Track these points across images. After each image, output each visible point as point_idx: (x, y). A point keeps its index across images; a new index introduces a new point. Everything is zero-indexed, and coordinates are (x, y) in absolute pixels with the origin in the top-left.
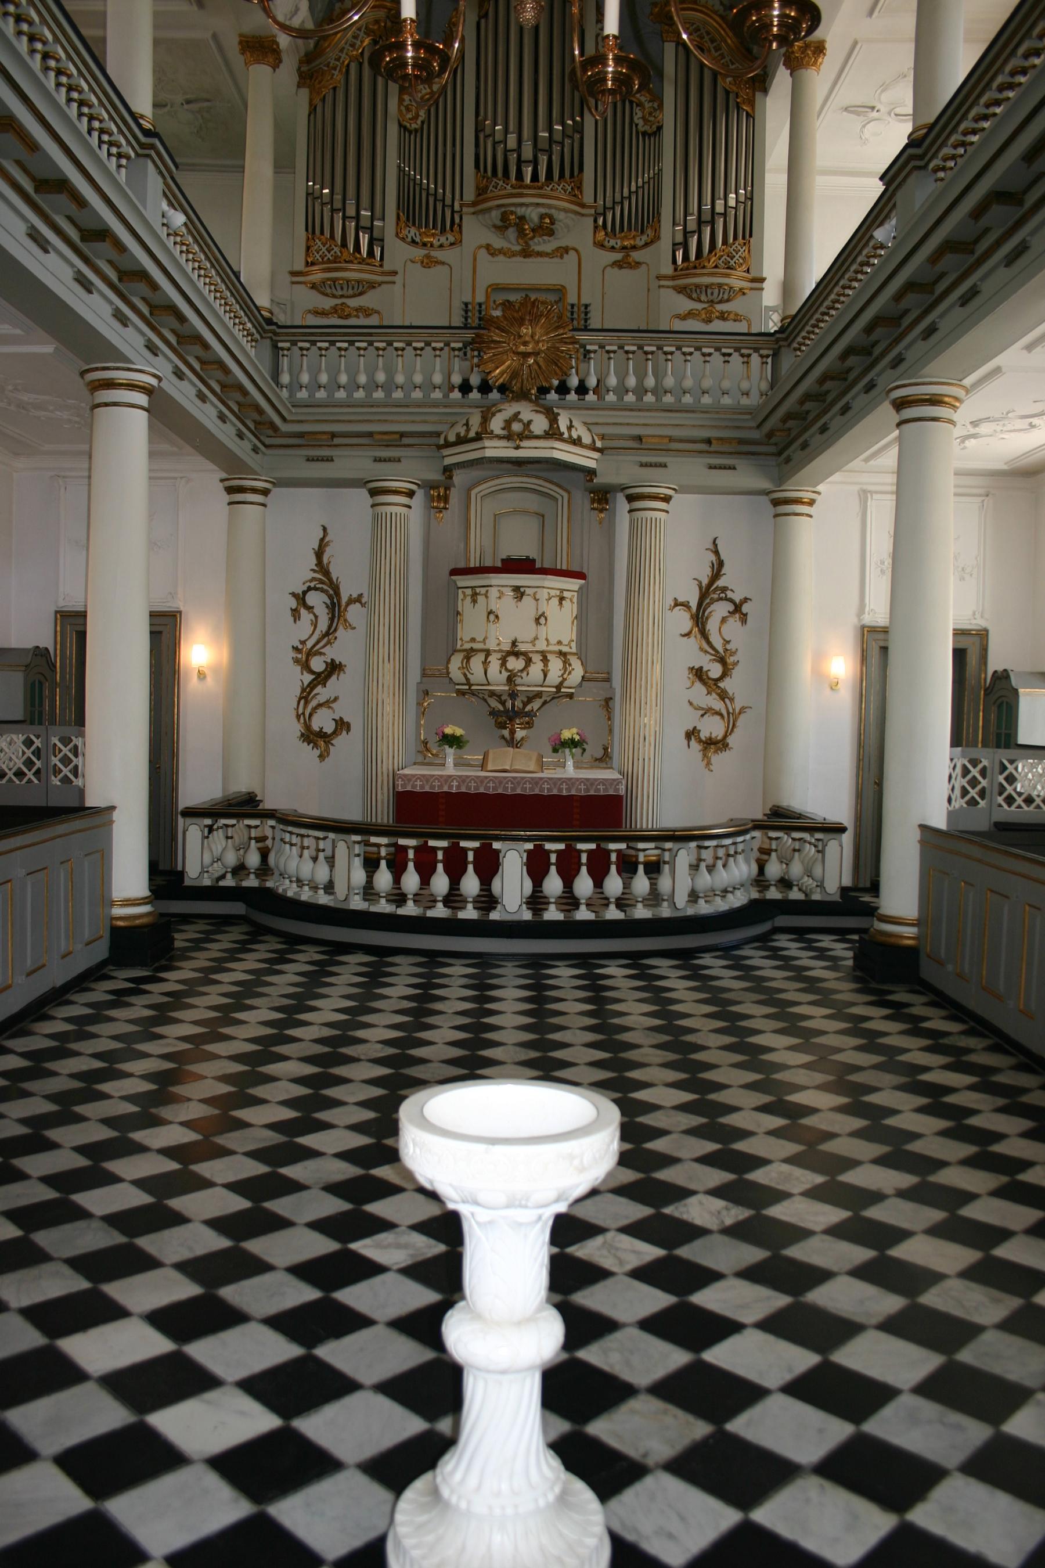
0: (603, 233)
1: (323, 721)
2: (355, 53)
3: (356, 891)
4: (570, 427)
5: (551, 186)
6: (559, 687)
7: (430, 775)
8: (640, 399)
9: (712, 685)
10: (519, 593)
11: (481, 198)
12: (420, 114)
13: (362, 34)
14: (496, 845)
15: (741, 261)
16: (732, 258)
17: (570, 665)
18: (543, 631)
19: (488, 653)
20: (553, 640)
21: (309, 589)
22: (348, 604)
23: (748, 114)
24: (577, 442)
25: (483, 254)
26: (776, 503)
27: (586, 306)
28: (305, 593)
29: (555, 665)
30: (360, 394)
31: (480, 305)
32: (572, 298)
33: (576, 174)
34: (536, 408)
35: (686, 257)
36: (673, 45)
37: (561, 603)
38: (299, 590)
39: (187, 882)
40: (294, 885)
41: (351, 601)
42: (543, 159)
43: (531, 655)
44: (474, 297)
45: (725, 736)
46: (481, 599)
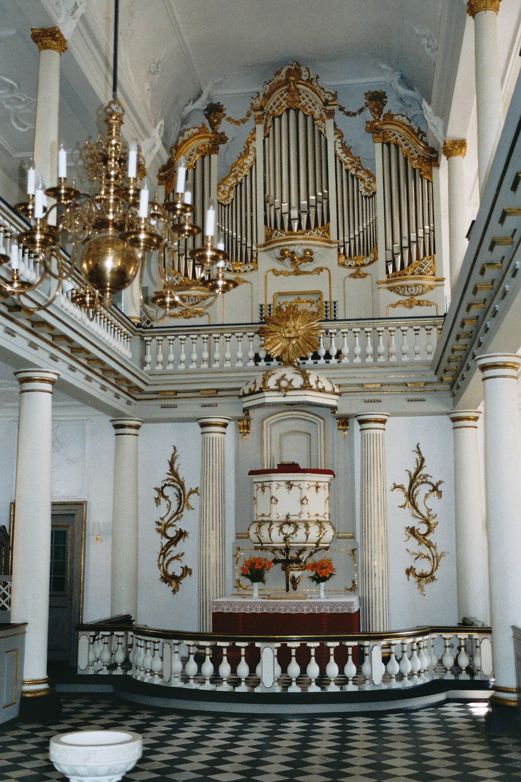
0: (344, 258)
1: (175, 569)
2: (191, 164)
3: (177, 675)
4: (317, 382)
5: (309, 233)
6: (317, 543)
7: (221, 602)
8: (363, 360)
9: (422, 538)
10: (290, 485)
11: (268, 242)
12: (231, 195)
13: (194, 153)
14: (257, 645)
15: (429, 269)
16: (423, 267)
17: (324, 529)
18: (305, 508)
19: (271, 523)
20: (313, 514)
21: (166, 485)
22: (190, 494)
23: (428, 181)
24: (322, 390)
25: (271, 275)
26: (454, 420)
27: (335, 303)
28: (163, 488)
29: (314, 531)
30: (193, 366)
31: (270, 306)
32: (326, 298)
33: (325, 224)
34: (296, 371)
35: (394, 269)
36: (380, 144)
37: (317, 490)
38: (159, 487)
39: (79, 672)
40: (148, 674)
41: (191, 492)
42: (304, 217)
43: (298, 524)
44: (266, 301)
45: (432, 572)
46: (267, 489)
